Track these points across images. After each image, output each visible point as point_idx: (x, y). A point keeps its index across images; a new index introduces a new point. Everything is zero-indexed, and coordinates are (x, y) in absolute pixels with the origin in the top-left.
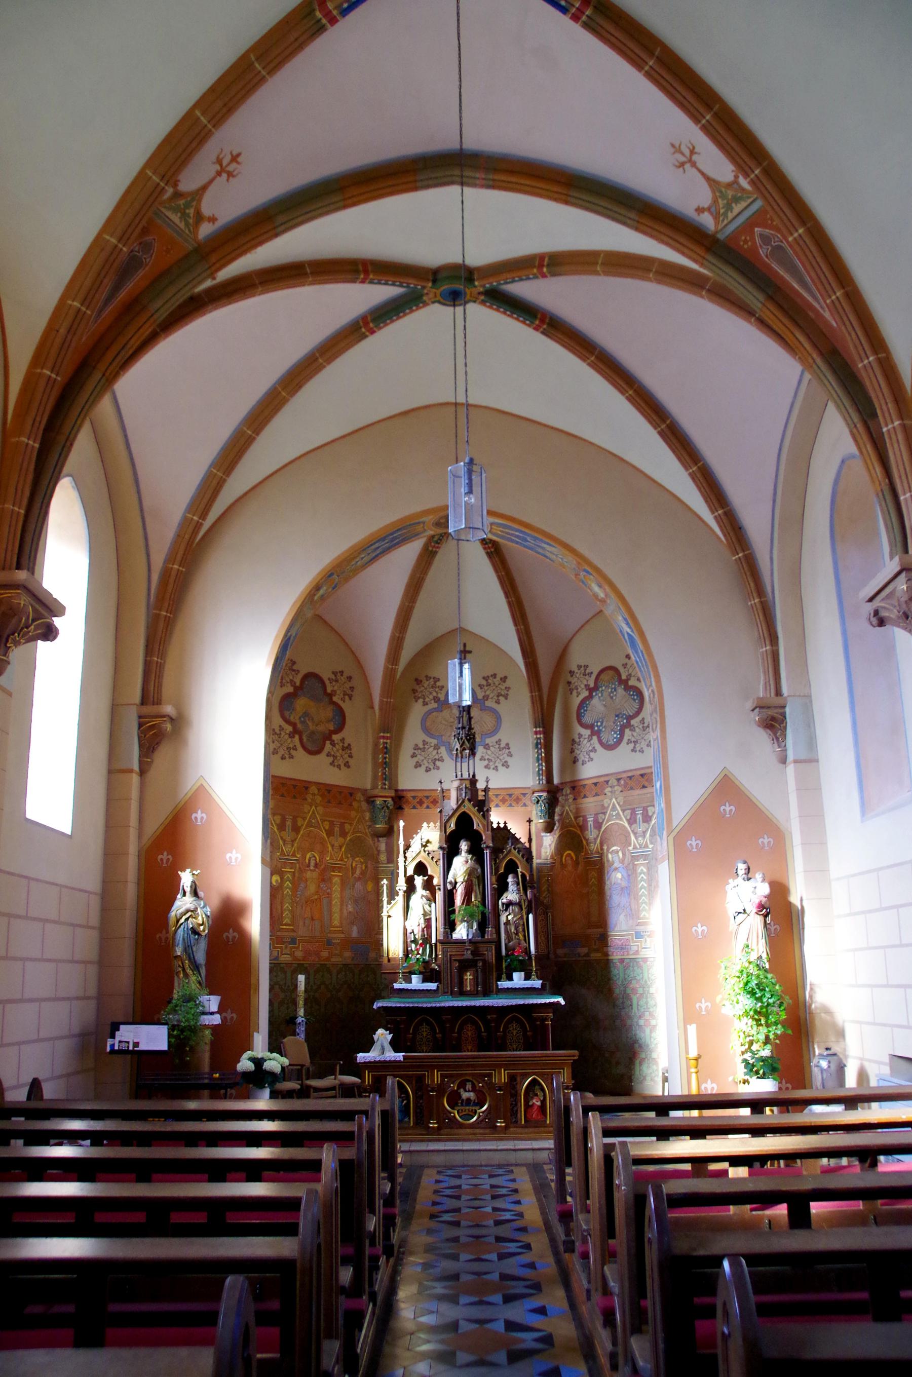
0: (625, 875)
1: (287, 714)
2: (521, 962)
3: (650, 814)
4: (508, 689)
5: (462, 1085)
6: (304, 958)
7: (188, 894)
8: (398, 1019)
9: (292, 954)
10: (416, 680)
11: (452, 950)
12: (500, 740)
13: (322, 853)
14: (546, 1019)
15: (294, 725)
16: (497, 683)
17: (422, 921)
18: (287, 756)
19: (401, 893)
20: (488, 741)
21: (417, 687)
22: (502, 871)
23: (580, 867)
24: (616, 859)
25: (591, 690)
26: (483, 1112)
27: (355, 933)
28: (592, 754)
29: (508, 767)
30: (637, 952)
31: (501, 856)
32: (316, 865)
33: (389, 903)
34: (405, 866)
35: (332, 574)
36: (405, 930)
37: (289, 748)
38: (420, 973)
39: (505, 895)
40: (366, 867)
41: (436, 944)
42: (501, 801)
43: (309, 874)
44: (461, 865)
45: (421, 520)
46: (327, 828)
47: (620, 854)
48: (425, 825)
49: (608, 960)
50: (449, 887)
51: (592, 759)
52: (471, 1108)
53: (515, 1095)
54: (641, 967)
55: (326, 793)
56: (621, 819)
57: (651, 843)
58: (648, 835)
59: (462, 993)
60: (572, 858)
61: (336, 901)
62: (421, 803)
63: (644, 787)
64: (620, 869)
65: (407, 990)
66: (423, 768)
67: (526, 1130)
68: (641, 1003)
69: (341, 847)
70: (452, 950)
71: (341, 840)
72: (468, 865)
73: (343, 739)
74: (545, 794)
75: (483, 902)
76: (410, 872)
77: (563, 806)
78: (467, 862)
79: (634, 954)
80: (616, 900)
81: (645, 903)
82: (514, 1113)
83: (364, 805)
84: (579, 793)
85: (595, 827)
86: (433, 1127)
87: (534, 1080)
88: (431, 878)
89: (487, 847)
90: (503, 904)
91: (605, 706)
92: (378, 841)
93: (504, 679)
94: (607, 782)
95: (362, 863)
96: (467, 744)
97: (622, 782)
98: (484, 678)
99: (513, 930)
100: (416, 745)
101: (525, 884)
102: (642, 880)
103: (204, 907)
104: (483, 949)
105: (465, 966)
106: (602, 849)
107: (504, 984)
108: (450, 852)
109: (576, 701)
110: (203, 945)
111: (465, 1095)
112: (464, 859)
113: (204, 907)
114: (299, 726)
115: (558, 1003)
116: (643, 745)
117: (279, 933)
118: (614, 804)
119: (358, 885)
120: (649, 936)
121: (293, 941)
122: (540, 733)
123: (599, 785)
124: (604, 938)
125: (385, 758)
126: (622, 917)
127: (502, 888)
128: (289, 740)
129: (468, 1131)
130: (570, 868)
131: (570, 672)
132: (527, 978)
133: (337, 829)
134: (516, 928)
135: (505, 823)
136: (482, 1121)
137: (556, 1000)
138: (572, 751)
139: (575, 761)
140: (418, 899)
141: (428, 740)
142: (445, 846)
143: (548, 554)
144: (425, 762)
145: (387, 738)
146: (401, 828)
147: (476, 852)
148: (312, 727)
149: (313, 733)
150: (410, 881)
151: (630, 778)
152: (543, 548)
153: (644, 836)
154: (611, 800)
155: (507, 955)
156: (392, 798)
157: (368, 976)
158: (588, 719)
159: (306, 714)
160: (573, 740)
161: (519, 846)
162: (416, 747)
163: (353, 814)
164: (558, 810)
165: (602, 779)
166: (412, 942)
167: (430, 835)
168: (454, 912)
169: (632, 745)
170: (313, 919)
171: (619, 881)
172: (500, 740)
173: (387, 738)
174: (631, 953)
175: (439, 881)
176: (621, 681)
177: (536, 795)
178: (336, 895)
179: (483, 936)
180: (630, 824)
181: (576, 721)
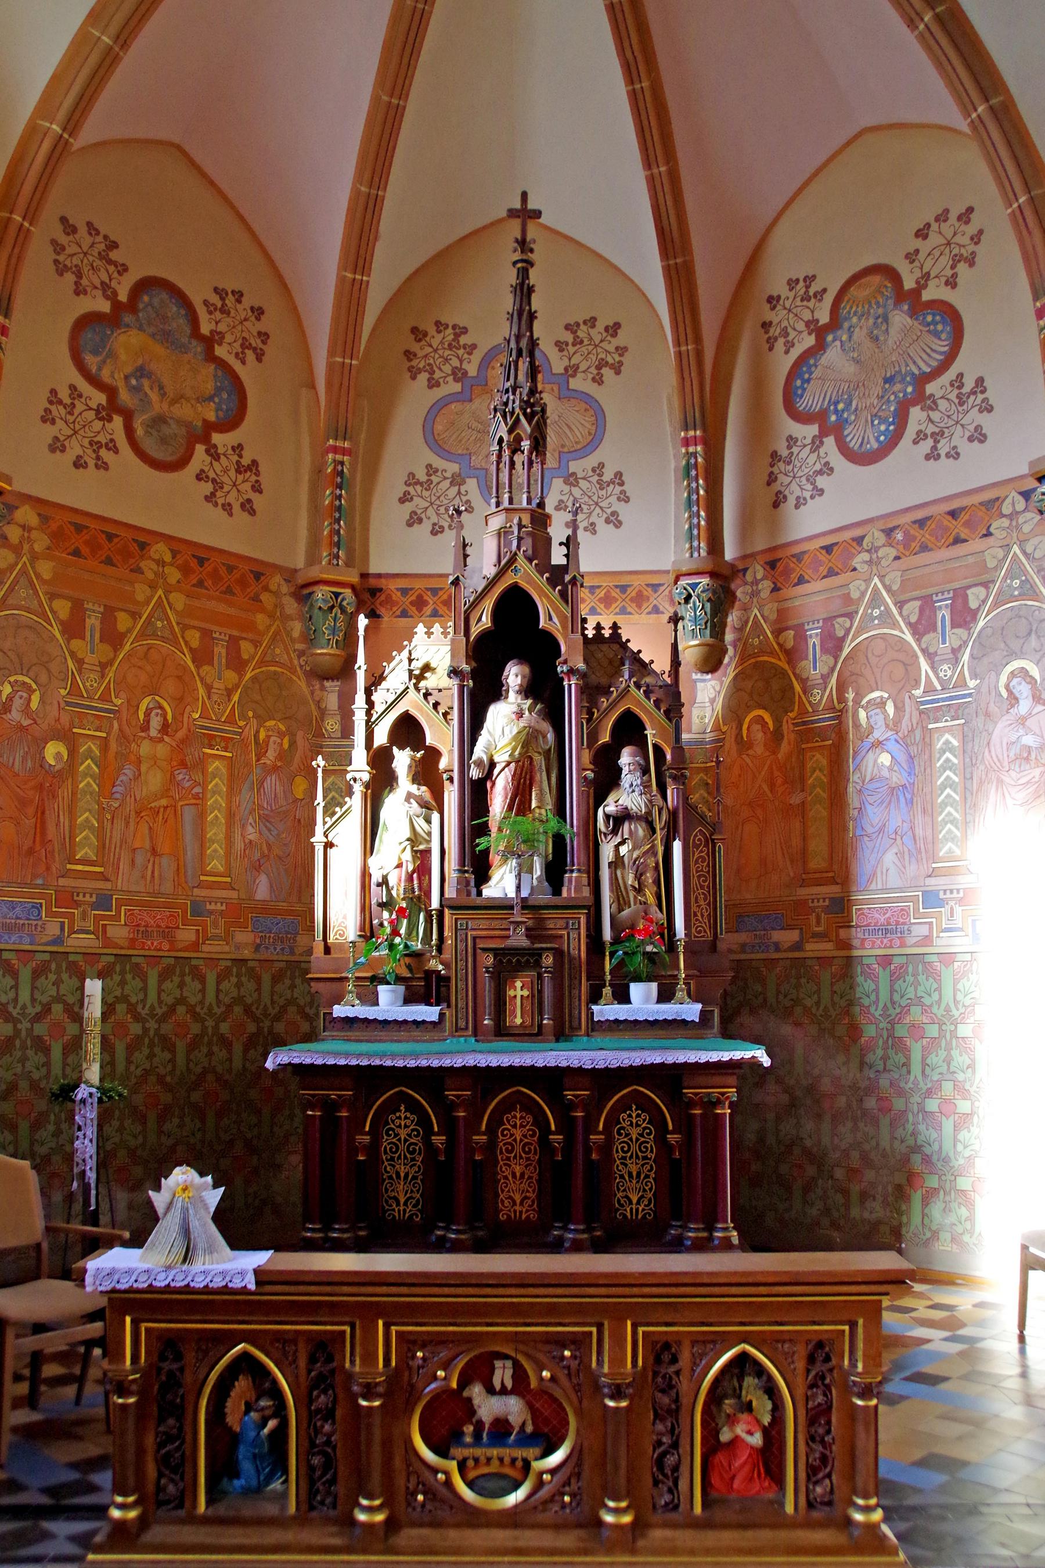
0: (902, 758)
1: (91, 361)
2: (650, 957)
3: (973, 604)
4: (622, 350)
5: (479, 1371)
6: (132, 943)
8: (333, 1095)
9: (101, 933)
10: (414, 330)
11: (479, 925)
12: (602, 465)
13: (180, 702)
14: (718, 1103)
15: (111, 392)
16: (597, 339)
17: (407, 856)
18: (91, 463)
19: (358, 789)
20: (574, 466)
21: (415, 347)
22: (605, 738)
23: (785, 747)
24: (879, 720)
25: (821, 332)
26: (553, 1471)
27: (262, 891)
28: (821, 481)
29: (618, 524)
30: (927, 940)
31: (604, 703)
32: (165, 728)
33: (328, 811)
34: (370, 722)
36: (365, 874)
37: (96, 446)
38: (399, 980)
39: (611, 799)
40: (293, 743)
41: (441, 914)
42: (600, 600)
43: (145, 748)
44: (504, 723)
46: (195, 644)
47: (890, 708)
48: (421, 629)
49: (849, 959)
50: (475, 773)
51: (821, 492)
52: (506, 1453)
53: (672, 1413)
54: (937, 977)
55: (194, 564)
56: (895, 625)
57: (974, 676)
58: (966, 657)
59: (501, 1031)
60: (764, 724)
61: (216, 816)
62: (420, 603)
63: (958, 541)
64: (891, 745)
65: (366, 1020)
66: (426, 526)
67: (711, 1538)
68: (932, 1059)
69: (229, 693)
70: (479, 925)
71: (231, 676)
72: (522, 723)
73: (240, 446)
74: (705, 581)
75: (560, 811)
76: (381, 738)
77: (746, 609)
78: (520, 715)
79: (916, 945)
80: (874, 817)
81: (953, 822)
82: (667, 1474)
83: (291, 606)
84: (787, 572)
85: (825, 650)
86: (369, 1526)
87: (742, 1361)
88: (434, 754)
89: (571, 672)
90: (607, 817)
91: (857, 361)
92: (323, 688)
93: (614, 329)
94: (859, 540)
95: (281, 735)
96: (526, 427)
97: (899, 536)
98: (567, 327)
99: (630, 879)
100: (412, 475)
101: (661, 771)
102: (948, 765)
104: (554, 923)
105: (509, 963)
106: (841, 699)
107: (607, 1011)
108: (481, 691)
109: (783, 362)
111: (488, 1407)
112: (515, 708)
114: (124, 397)
115: (754, 1064)
116: (959, 438)
117: (62, 882)
118: (876, 589)
119: (272, 783)
120: (960, 902)
121: (103, 902)
122: (695, 441)
123: (838, 552)
124: (841, 908)
126: (890, 858)
127: (606, 779)
128: (98, 425)
129: (501, 1536)
130: (759, 749)
131: (770, 299)
132: (665, 996)
133: (220, 650)
134: (639, 876)
135: (615, 627)
136: (552, 1499)
137: (748, 1055)
138: (772, 479)
140: (398, 809)
141: (438, 463)
142: (465, 667)
144: (431, 512)
145: (344, 452)
146: (361, 633)
147: (544, 690)
148: (158, 406)
149: (160, 420)
150: (380, 760)
151: (921, 523)
153: (956, 661)
154: (868, 581)
155: (616, 941)
156: (353, 588)
157: (293, 987)
158: (811, 400)
159: (141, 372)
160: (774, 455)
161: (648, 680)
162: (412, 480)
163: (261, 619)
164: (733, 619)
165: (847, 535)
166: (382, 905)
167: (434, 649)
168: (483, 830)
169: (926, 445)
170: (154, 852)
171: (885, 773)
172: (602, 465)
173: (344, 452)
174: (911, 941)
175: (451, 761)
176: (901, 295)
177: (683, 582)
178: (216, 801)
179: (557, 891)
180: (917, 631)
181: (783, 412)
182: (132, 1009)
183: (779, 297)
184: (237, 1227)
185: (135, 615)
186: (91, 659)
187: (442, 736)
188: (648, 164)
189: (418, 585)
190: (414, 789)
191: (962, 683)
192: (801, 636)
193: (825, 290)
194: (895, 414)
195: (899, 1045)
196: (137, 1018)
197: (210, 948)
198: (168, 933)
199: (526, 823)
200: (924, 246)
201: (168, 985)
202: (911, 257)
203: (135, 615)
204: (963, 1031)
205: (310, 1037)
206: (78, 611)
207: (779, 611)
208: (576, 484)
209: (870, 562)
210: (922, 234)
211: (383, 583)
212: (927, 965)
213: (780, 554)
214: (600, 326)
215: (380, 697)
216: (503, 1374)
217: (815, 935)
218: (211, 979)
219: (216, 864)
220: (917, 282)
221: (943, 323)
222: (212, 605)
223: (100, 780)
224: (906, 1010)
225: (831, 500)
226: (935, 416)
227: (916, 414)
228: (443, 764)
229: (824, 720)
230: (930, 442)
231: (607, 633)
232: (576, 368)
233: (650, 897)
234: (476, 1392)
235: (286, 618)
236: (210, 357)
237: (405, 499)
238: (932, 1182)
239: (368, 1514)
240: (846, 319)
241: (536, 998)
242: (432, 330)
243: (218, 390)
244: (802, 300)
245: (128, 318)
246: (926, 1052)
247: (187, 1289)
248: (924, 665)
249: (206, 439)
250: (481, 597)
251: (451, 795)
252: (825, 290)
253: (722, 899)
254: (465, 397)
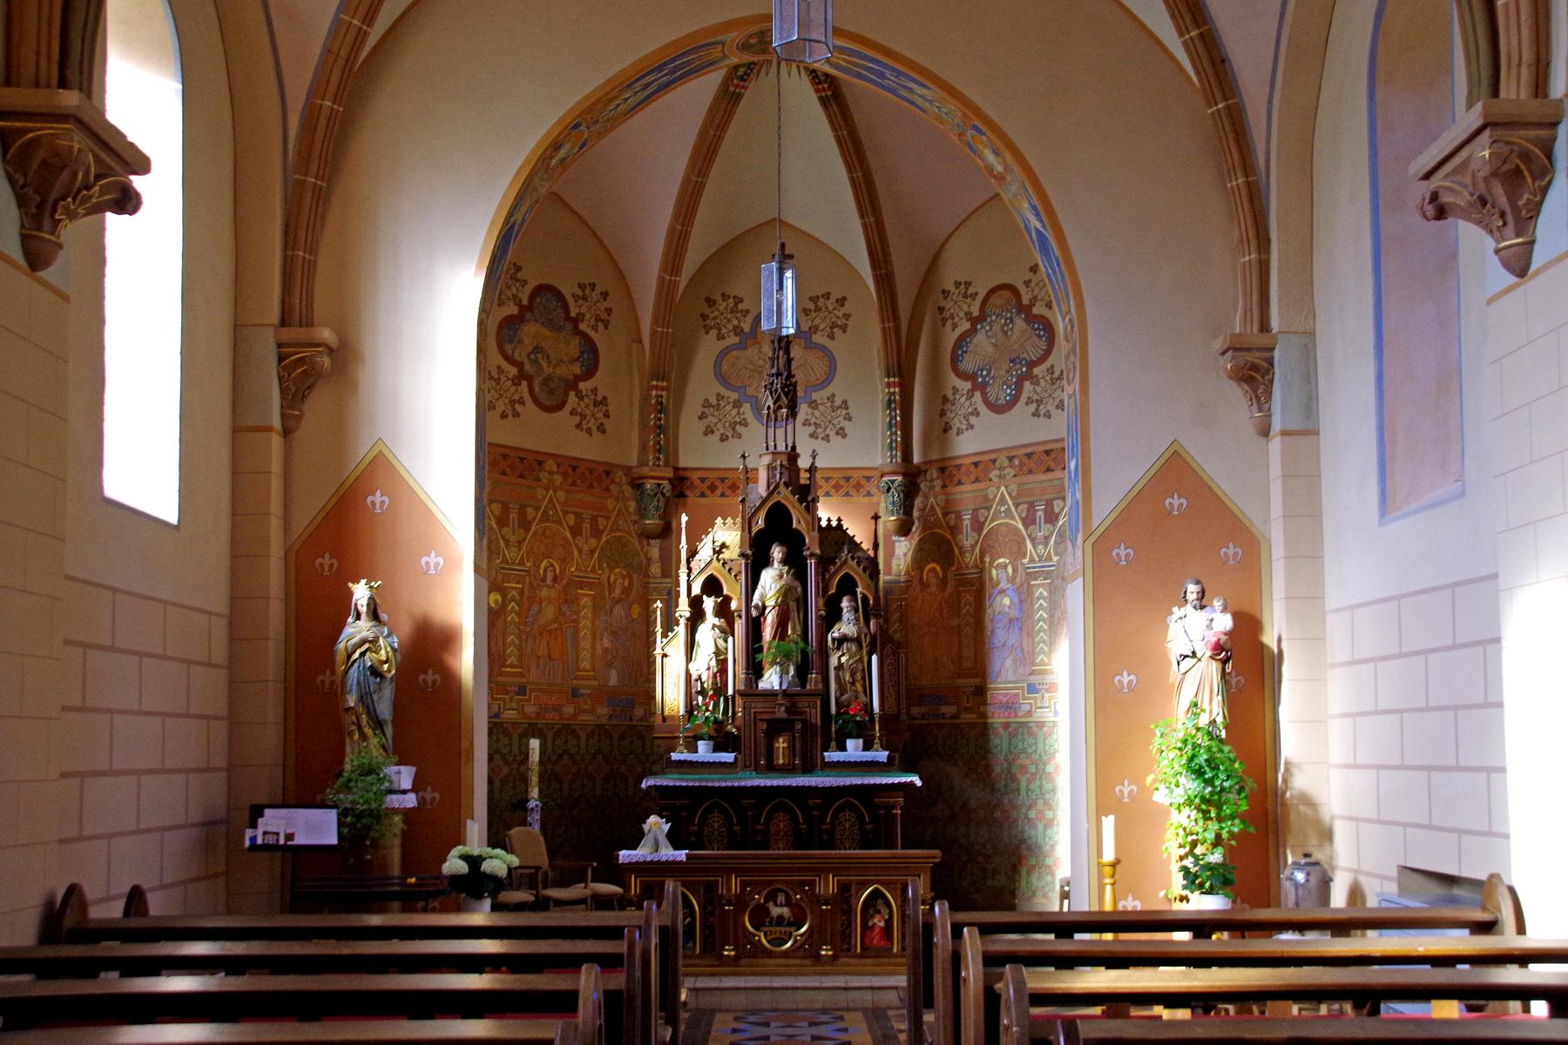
0: (1016, 601)
1: (508, 348)
3: (1057, 510)
4: (847, 316)
5: (771, 896)
6: (538, 714)
7: (363, 616)
9: (520, 709)
10: (708, 300)
11: (758, 706)
12: (833, 395)
14: (894, 807)
15: (520, 365)
17: (713, 663)
19: (682, 622)
20: (815, 396)
21: (707, 311)
23: (949, 589)
24: (1003, 576)
28: (973, 420)
29: (844, 436)
30: (1029, 713)
31: (832, 569)
32: (555, 579)
33: (664, 635)
34: (689, 582)
35: (577, 125)
37: (512, 402)
38: (710, 738)
40: (630, 583)
41: (733, 697)
43: (544, 593)
44: (770, 582)
45: (720, 38)
47: (1010, 570)
50: (754, 613)
53: (848, 912)
54: (1034, 736)
56: (1013, 518)
59: (771, 768)
61: (585, 633)
63: (1049, 470)
64: (1010, 592)
65: (691, 762)
66: (716, 436)
67: (863, 961)
69: (592, 552)
70: (758, 706)
71: (593, 542)
76: (696, 590)
77: (926, 497)
78: (781, 577)
80: (1001, 636)
82: (846, 936)
83: (628, 491)
84: (951, 476)
87: (876, 894)
89: (812, 555)
91: (995, 345)
93: (842, 301)
94: (994, 461)
95: (624, 577)
96: (785, 400)
100: (707, 400)
101: (866, 611)
103: (389, 635)
104: (802, 704)
105: (775, 728)
106: (982, 561)
107: (832, 756)
108: (757, 561)
109: (951, 337)
110: (388, 691)
111: (776, 911)
113: (389, 635)
115: (912, 784)
116: (1051, 406)
119: (618, 610)
120: (1048, 690)
123: (982, 466)
124: (981, 692)
126: (1009, 662)
130: (933, 589)
131: (944, 292)
134: (853, 675)
138: (943, 414)
139: (946, 429)
140: (707, 634)
141: (724, 392)
143: (919, 101)
145: (663, 389)
147: (795, 561)
150: (696, 603)
151: (1029, 455)
152: (910, 90)
153: (1046, 544)
158: (968, 365)
159: (537, 349)
160: (945, 398)
162: (707, 404)
163: (610, 503)
164: (918, 502)
165: (987, 457)
166: (698, 693)
167: (727, 535)
169: (1033, 407)
170: (550, 658)
172: (833, 395)
173: (663, 389)
175: (739, 604)
177: (886, 479)
178: (585, 624)
179: (803, 686)
180: (1026, 526)
182: (503, 757)
184: (675, 840)
185: (537, 509)
186: (513, 539)
187: (733, 589)
188: (862, 216)
189: (712, 475)
190: (716, 621)
191: (1049, 558)
192: (959, 518)
194: (1016, 384)
195: (1014, 779)
196: (507, 763)
197: (585, 718)
198: (558, 709)
199: (785, 645)
201: (558, 741)
203: (537, 509)
204: (1049, 769)
205: (662, 772)
206: (506, 510)
207: (947, 501)
208: (816, 408)
209: (1000, 476)
211: (688, 474)
212: (1029, 729)
213: (947, 463)
214: (833, 299)
215: (696, 565)
216: (781, 898)
217: (966, 709)
218: (583, 736)
219: (586, 664)
222: (580, 496)
223: (519, 615)
224: (1017, 757)
225: (977, 436)
226: (1038, 389)
227: (1027, 386)
228: (734, 605)
229: (972, 573)
230: (1034, 406)
231: (834, 523)
232: (816, 328)
233: (859, 687)
234: (771, 905)
235: (625, 500)
236: (577, 332)
237: (702, 417)
238: (1032, 861)
239: (728, 952)
241: (791, 748)
242: (720, 300)
243: (582, 352)
245: (529, 315)
246: (1029, 782)
247: (659, 862)
248: (1029, 545)
249: (575, 387)
250: (758, 510)
251: (740, 626)
253: (903, 688)
254: (742, 347)
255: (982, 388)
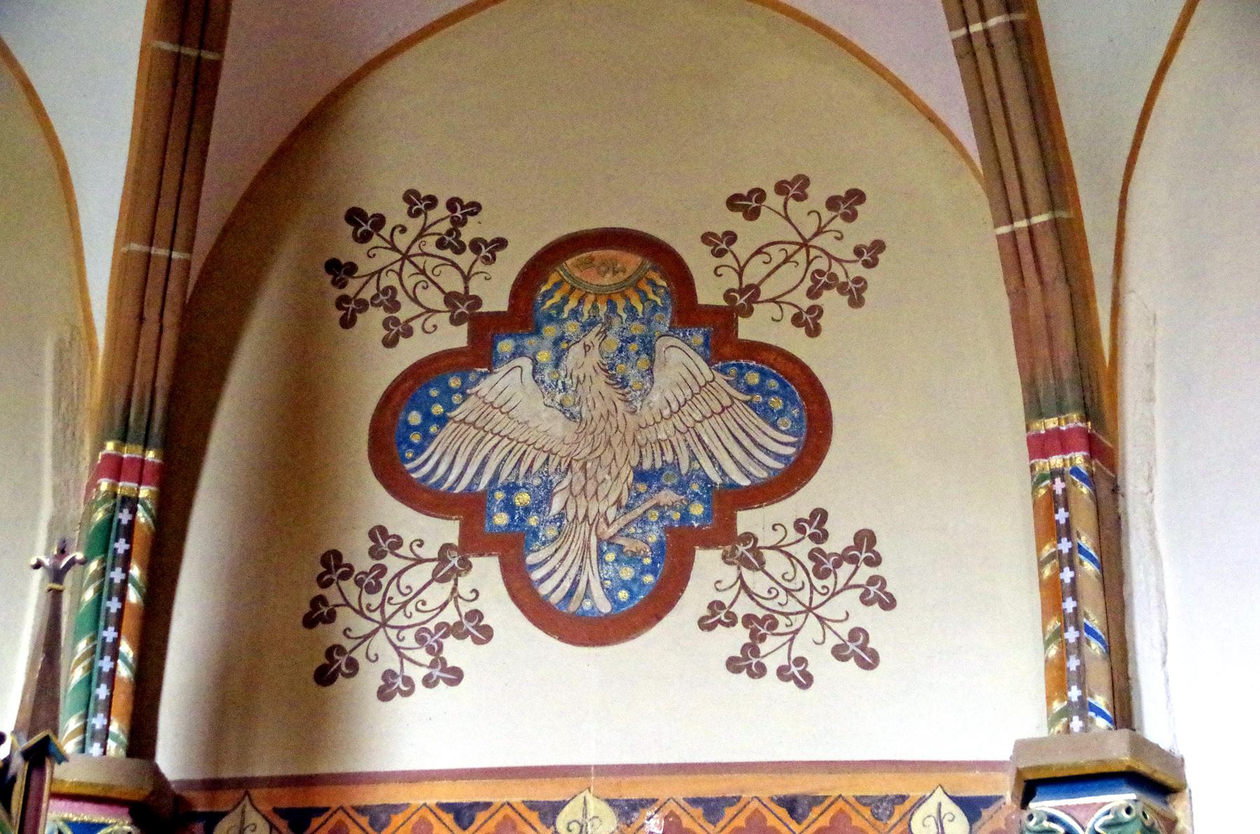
4: (871, 253)
28: (456, 651)
29: (869, 660)
93: (849, 203)
109: (373, 365)
116: (812, 645)
125: (131, 502)
131: (355, 216)
139: (331, 670)
158: (447, 459)
160: (334, 565)
165: (517, 793)
172: (820, 516)
176: (687, 312)
183: (379, 221)
193: (501, 243)
200: (750, 234)
202: (720, 243)
210: (746, 204)
220: (727, 296)
221: (787, 398)
230: (741, 635)
240: (550, 319)
244: (441, 244)
252: (501, 243)
255: (512, 551)
